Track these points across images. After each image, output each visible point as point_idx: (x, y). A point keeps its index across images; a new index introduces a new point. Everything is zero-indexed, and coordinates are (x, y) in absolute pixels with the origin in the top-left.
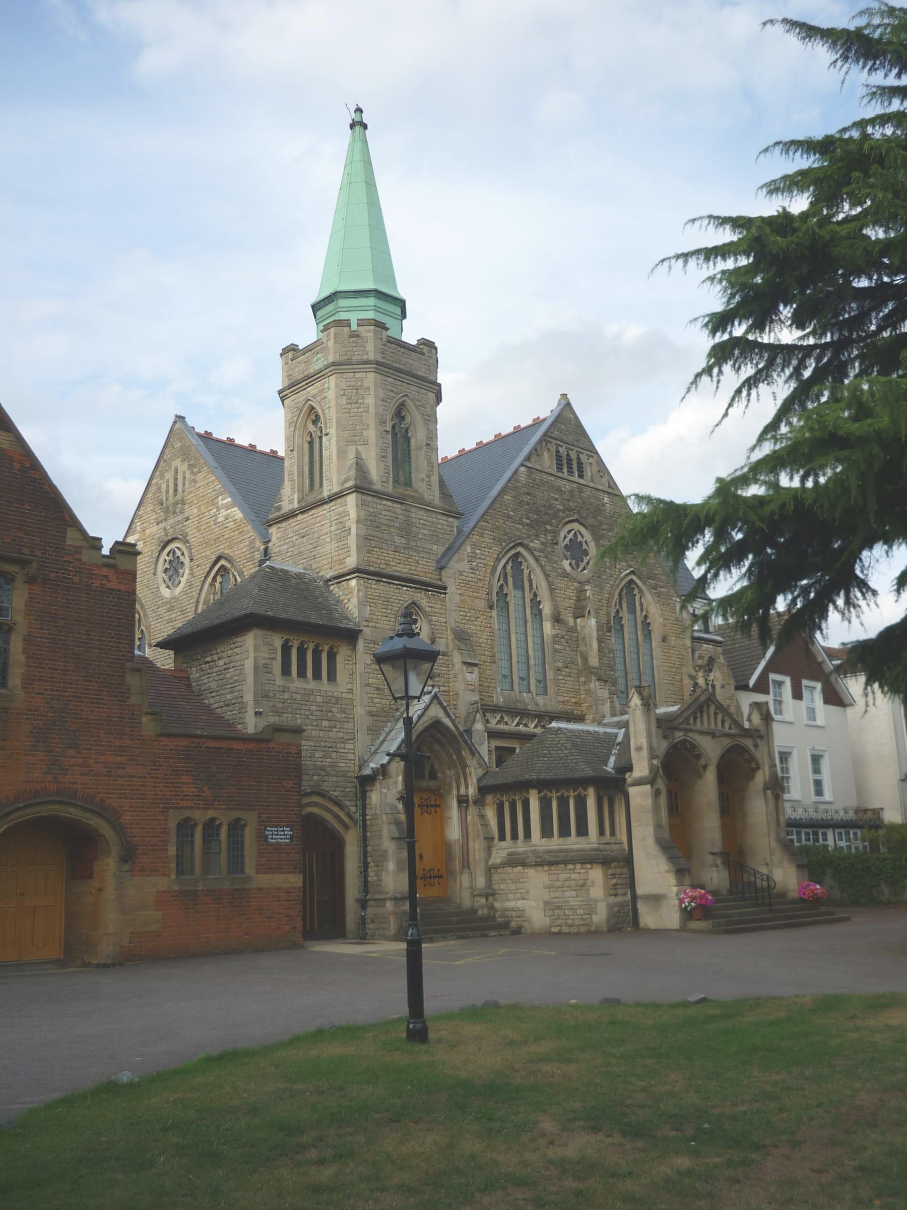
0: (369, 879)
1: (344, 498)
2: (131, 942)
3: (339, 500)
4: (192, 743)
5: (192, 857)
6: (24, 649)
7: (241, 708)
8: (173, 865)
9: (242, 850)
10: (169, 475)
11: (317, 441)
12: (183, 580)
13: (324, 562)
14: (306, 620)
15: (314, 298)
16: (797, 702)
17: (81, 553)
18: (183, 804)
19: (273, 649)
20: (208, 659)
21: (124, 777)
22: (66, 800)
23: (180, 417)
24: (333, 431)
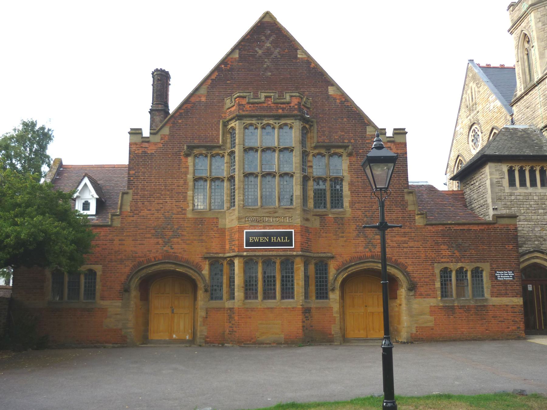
1: (545, 81)
2: (417, 332)
3: (542, 83)
4: (446, 228)
5: (451, 288)
6: (349, 188)
8: (439, 293)
10: (469, 92)
12: (480, 144)
13: (539, 120)
14: (522, 153)
20: (472, 183)
21: (407, 247)
22: (376, 261)
23: (470, 60)
24: (535, 44)
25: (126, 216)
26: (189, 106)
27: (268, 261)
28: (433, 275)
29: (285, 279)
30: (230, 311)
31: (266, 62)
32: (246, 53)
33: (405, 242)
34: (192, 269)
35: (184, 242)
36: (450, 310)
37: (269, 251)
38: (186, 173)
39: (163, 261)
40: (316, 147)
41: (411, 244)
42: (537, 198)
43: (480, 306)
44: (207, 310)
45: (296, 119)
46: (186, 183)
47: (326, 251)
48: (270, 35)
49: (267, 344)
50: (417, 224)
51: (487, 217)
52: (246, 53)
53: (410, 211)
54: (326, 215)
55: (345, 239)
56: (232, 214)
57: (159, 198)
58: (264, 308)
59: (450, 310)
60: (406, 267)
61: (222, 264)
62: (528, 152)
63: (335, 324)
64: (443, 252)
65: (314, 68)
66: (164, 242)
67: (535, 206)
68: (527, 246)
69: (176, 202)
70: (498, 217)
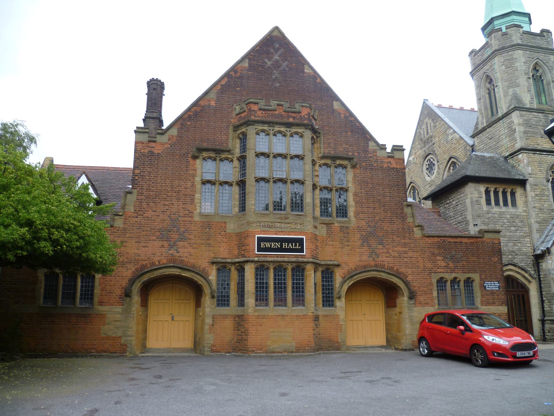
0: (545, 309)
1: (510, 115)
3: (508, 117)
7: (466, 223)
8: (436, 301)
9: (473, 293)
10: (424, 126)
11: (492, 91)
12: (435, 172)
15: (483, 24)
17: (376, 152)
18: (439, 270)
19: (480, 193)
20: (448, 202)
22: (380, 269)
24: (499, 84)
25: (129, 217)
26: (198, 109)
27: (280, 269)
28: (431, 284)
29: (259, 285)
30: (239, 318)
31: (274, 73)
32: (255, 63)
33: (405, 253)
35: (190, 246)
37: (281, 257)
38: (194, 176)
39: (168, 265)
40: (323, 157)
41: (410, 254)
44: (214, 317)
45: (306, 129)
47: (333, 259)
49: (278, 352)
50: (415, 236)
51: (466, 233)
52: (255, 63)
53: (409, 223)
54: (332, 224)
56: (241, 219)
57: (165, 199)
58: (276, 316)
61: (230, 270)
62: (500, 175)
63: (341, 332)
64: (439, 262)
65: (320, 83)
66: (169, 245)
69: (183, 204)
70: (483, 232)
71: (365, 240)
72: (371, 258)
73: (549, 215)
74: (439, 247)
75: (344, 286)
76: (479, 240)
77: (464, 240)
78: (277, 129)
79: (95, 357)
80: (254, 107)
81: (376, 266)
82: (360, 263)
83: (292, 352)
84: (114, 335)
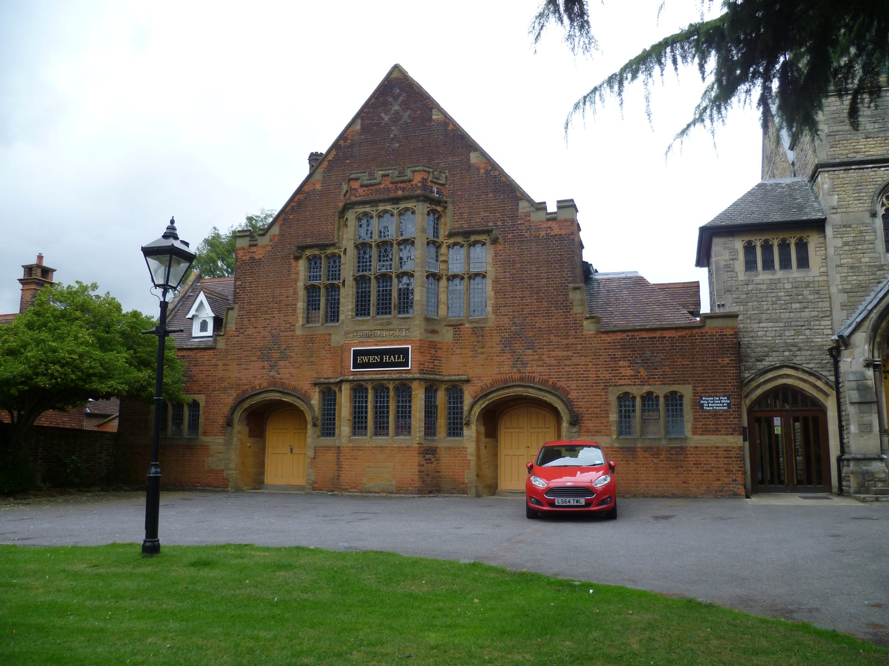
8: (614, 428)
16: (154, 236)
18: (621, 382)
19: (734, 252)
27: (380, 388)
28: (607, 403)
29: (400, 409)
32: (369, 122)
34: (299, 398)
36: (630, 452)
38: (296, 281)
40: (451, 235)
41: (575, 360)
42: (790, 286)
43: (676, 448)
44: (315, 449)
46: (295, 293)
48: (399, 95)
49: (375, 492)
52: (369, 122)
53: (576, 314)
55: (486, 355)
57: (266, 312)
59: (630, 452)
60: (568, 393)
63: (469, 469)
64: (622, 370)
65: (453, 130)
67: (785, 298)
68: (770, 359)
71: (507, 344)
72: (515, 369)
73: (872, 277)
74: (624, 347)
75: (475, 409)
76: (695, 331)
77: (667, 334)
78: (381, 208)
79: (200, 491)
80: (355, 185)
81: (522, 379)
82: (499, 377)
83: (392, 493)
84: (217, 468)
